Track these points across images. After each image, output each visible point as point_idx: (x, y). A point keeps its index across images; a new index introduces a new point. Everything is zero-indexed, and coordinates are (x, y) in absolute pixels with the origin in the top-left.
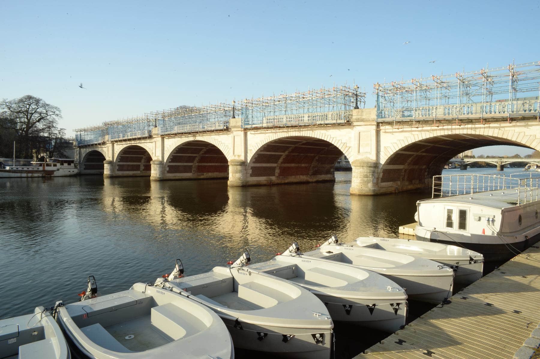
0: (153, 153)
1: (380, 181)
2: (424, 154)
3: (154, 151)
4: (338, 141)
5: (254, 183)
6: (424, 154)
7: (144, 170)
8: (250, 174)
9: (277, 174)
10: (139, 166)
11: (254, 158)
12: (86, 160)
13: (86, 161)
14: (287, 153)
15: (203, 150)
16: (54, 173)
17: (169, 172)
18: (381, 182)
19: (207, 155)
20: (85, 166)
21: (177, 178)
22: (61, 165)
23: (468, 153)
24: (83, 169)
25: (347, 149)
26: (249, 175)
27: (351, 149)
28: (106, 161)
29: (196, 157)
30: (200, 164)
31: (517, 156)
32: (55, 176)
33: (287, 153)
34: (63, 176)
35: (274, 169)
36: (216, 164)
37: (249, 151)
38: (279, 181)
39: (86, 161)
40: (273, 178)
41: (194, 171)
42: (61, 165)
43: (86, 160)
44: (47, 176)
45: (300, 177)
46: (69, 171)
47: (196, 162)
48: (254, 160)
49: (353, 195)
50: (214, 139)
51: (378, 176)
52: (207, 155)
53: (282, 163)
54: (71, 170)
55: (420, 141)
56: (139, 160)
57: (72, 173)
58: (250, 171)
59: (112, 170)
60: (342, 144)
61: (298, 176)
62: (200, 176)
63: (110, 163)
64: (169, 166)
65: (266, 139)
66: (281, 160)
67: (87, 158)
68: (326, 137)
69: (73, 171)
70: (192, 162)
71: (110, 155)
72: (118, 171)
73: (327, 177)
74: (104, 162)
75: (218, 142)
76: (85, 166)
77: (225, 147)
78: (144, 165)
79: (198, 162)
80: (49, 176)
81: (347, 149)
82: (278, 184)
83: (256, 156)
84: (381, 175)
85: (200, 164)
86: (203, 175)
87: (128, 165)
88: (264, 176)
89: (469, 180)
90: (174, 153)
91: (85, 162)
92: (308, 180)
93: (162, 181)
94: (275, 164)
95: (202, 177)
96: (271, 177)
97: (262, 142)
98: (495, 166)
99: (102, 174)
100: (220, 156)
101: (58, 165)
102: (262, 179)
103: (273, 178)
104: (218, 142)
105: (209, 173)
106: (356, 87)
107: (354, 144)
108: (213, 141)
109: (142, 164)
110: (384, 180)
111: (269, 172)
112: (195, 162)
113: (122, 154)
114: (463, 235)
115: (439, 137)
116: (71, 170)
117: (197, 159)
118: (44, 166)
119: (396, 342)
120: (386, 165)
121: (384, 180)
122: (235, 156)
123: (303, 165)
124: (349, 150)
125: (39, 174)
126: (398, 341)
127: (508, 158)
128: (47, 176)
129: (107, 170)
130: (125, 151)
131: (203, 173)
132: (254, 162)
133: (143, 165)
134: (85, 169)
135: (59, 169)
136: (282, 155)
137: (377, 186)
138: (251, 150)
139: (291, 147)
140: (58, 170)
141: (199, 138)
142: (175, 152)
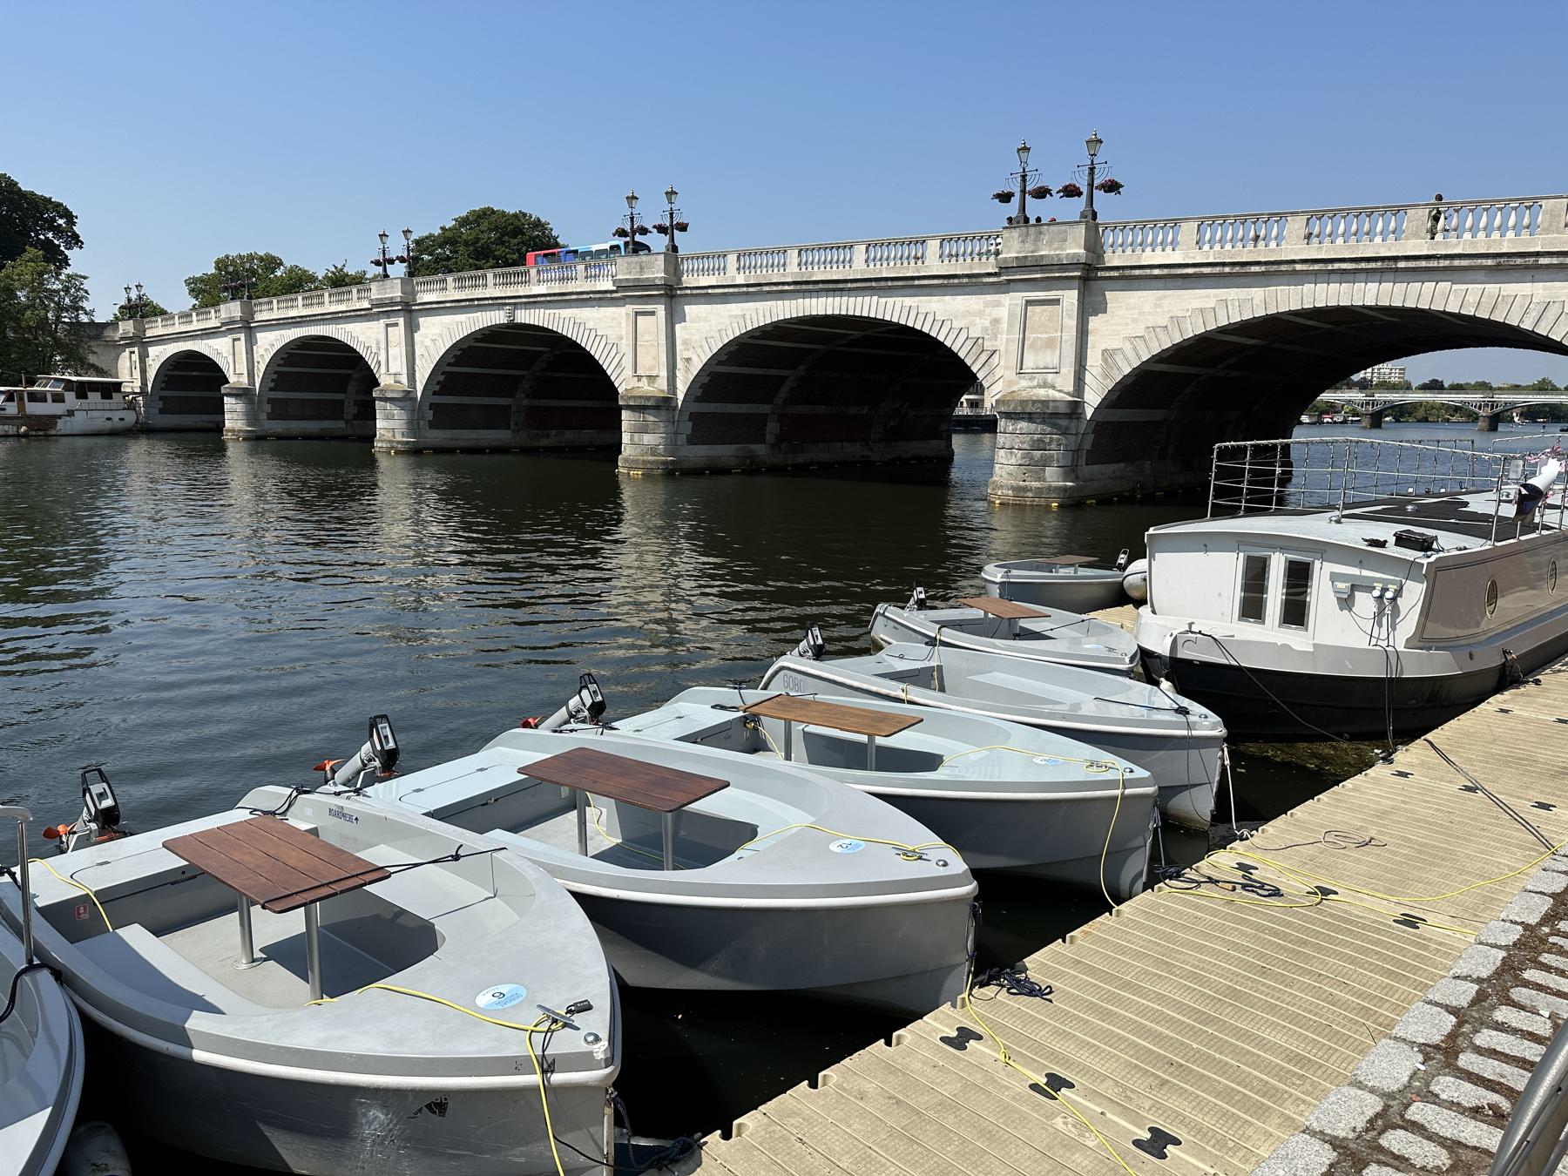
0: (379, 363)
1: (1083, 461)
2: (1235, 374)
3: (382, 358)
4: (956, 332)
6: (1235, 374)
7: (356, 417)
9: (769, 438)
11: (699, 385)
13: (272, 385)
14: (801, 370)
16: (56, 424)
19: (556, 375)
20: (161, 403)
22: (77, 398)
23: (1387, 370)
24: (157, 411)
25: (984, 357)
26: (682, 439)
27: (996, 356)
29: (522, 377)
30: (537, 403)
31: (1544, 387)
32: (62, 432)
33: (801, 370)
36: (589, 404)
37: (680, 364)
39: (272, 385)
40: (761, 450)
41: (517, 424)
42: (77, 398)
44: (34, 433)
46: (109, 419)
47: (523, 396)
48: (699, 392)
50: (572, 320)
52: (556, 375)
54: (116, 416)
55: (1222, 330)
56: (341, 384)
57: (116, 423)
58: (687, 427)
59: (251, 417)
60: (970, 343)
61: (838, 444)
63: (242, 394)
66: (783, 394)
67: (276, 372)
68: (921, 318)
69: (122, 419)
71: (243, 367)
73: (931, 447)
75: (587, 332)
76: (161, 403)
77: (609, 347)
78: (356, 403)
79: (527, 397)
80: (41, 433)
81: (984, 357)
85: (537, 403)
86: (548, 436)
87: (304, 401)
88: (731, 443)
90: (449, 364)
92: (868, 457)
93: (415, 452)
94: (765, 406)
96: (753, 447)
97: (724, 333)
98: (1472, 417)
99: (219, 428)
101: (70, 396)
102: (724, 452)
103: (761, 450)
104: (587, 332)
105: (567, 432)
107: (1006, 341)
108: (571, 330)
109: (349, 398)
110: (1095, 457)
111: (748, 429)
112: (520, 395)
114: (1286, 647)
115: (1285, 317)
116: (116, 416)
118: (21, 399)
119: (944, 1039)
120: (1106, 407)
121: (1095, 457)
122: (639, 378)
123: (853, 410)
124: (991, 360)
125: (6, 427)
126: (955, 1034)
127: (1516, 388)
128: (34, 433)
130: (290, 356)
131: (546, 432)
132: (698, 400)
133: (352, 403)
134: (162, 411)
135: (73, 411)
136: (788, 377)
137: (1073, 474)
138: (688, 360)
139: (815, 350)
140: (71, 413)
141: (525, 317)
142: (724, 358)
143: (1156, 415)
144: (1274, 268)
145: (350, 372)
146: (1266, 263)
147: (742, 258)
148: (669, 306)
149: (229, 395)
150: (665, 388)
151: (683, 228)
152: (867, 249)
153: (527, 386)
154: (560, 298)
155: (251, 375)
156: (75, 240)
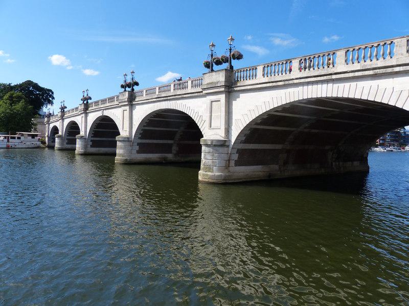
1: (232, 163)
9: (174, 152)
13: (93, 135)
17: (238, 163)
21: (102, 152)
28: (79, 135)
29: (177, 131)
33: (182, 129)
35: (170, 146)
38: (178, 159)
39: (93, 135)
48: (244, 138)
51: (229, 158)
64: (138, 144)
65: (275, 100)
72: (67, 144)
74: (117, 138)
83: (248, 132)
84: (235, 157)
87: (264, 150)
91: (92, 137)
93: (85, 155)
96: (166, 155)
113: (94, 128)
129: (121, 151)
134: (138, 152)
137: (226, 170)
142: (259, 121)
143: (278, 147)
144: (287, 82)
145: (177, 130)
146: (284, 81)
147: (266, 68)
148: (228, 96)
149: (120, 141)
150: (223, 135)
151: (137, 84)
152: (264, 68)
154: (147, 101)
155: (228, 131)
156: (53, 98)
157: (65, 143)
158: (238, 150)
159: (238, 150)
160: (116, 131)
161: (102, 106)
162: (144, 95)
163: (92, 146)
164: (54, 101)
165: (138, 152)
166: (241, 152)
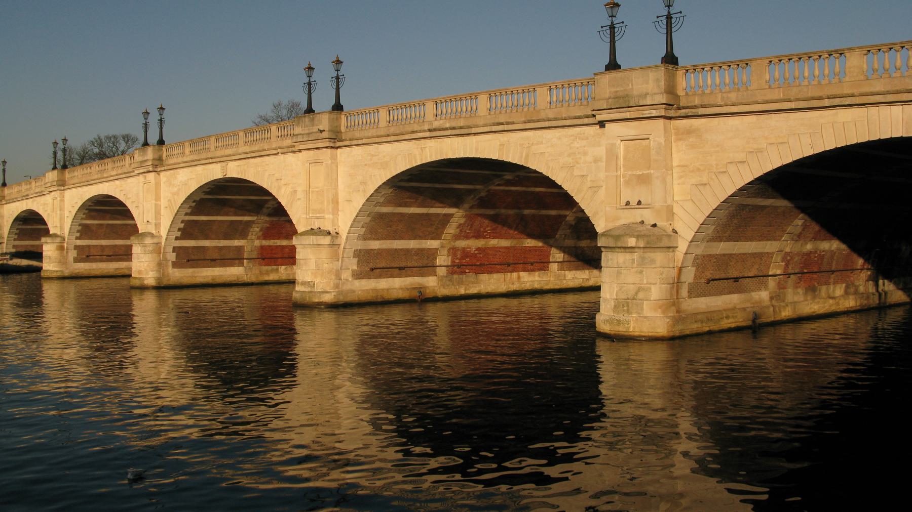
1: (684, 292)
5: (364, 297)
8: (353, 271)
10: (432, 254)
12: (16, 234)
13: (78, 235)
15: (267, 206)
17: (695, 292)
18: (690, 297)
29: (253, 222)
30: (266, 243)
34: (356, 310)
39: (78, 235)
43: (16, 234)
45: (519, 277)
48: (711, 229)
49: (634, 340)
53: (457, 237)
62: (268, 273)
64: (175, 249)
66: (451, 230)
67: (80, 225)
70: (243, 235)
79: (258, 238)
82: (446, 299)
84: (689, 276)
85: (266, 243)
89: (715, 283)
91: (177, 238)
95: (272, 277)
100: (20, 227)
106: (277, 103)
117: (256, 229)
131: (275, 267)
134: (358, 276)
147: (391, 112)
153: (257, 229)
157: (346, 275)
158: (174, 248)
159: (174, 248)
160: (43, 227)
161: (114, 173)
162: (242, 142)
163: (175, 265)
164: (285, 102)
165: (358, 276)
166: (702, 263)
